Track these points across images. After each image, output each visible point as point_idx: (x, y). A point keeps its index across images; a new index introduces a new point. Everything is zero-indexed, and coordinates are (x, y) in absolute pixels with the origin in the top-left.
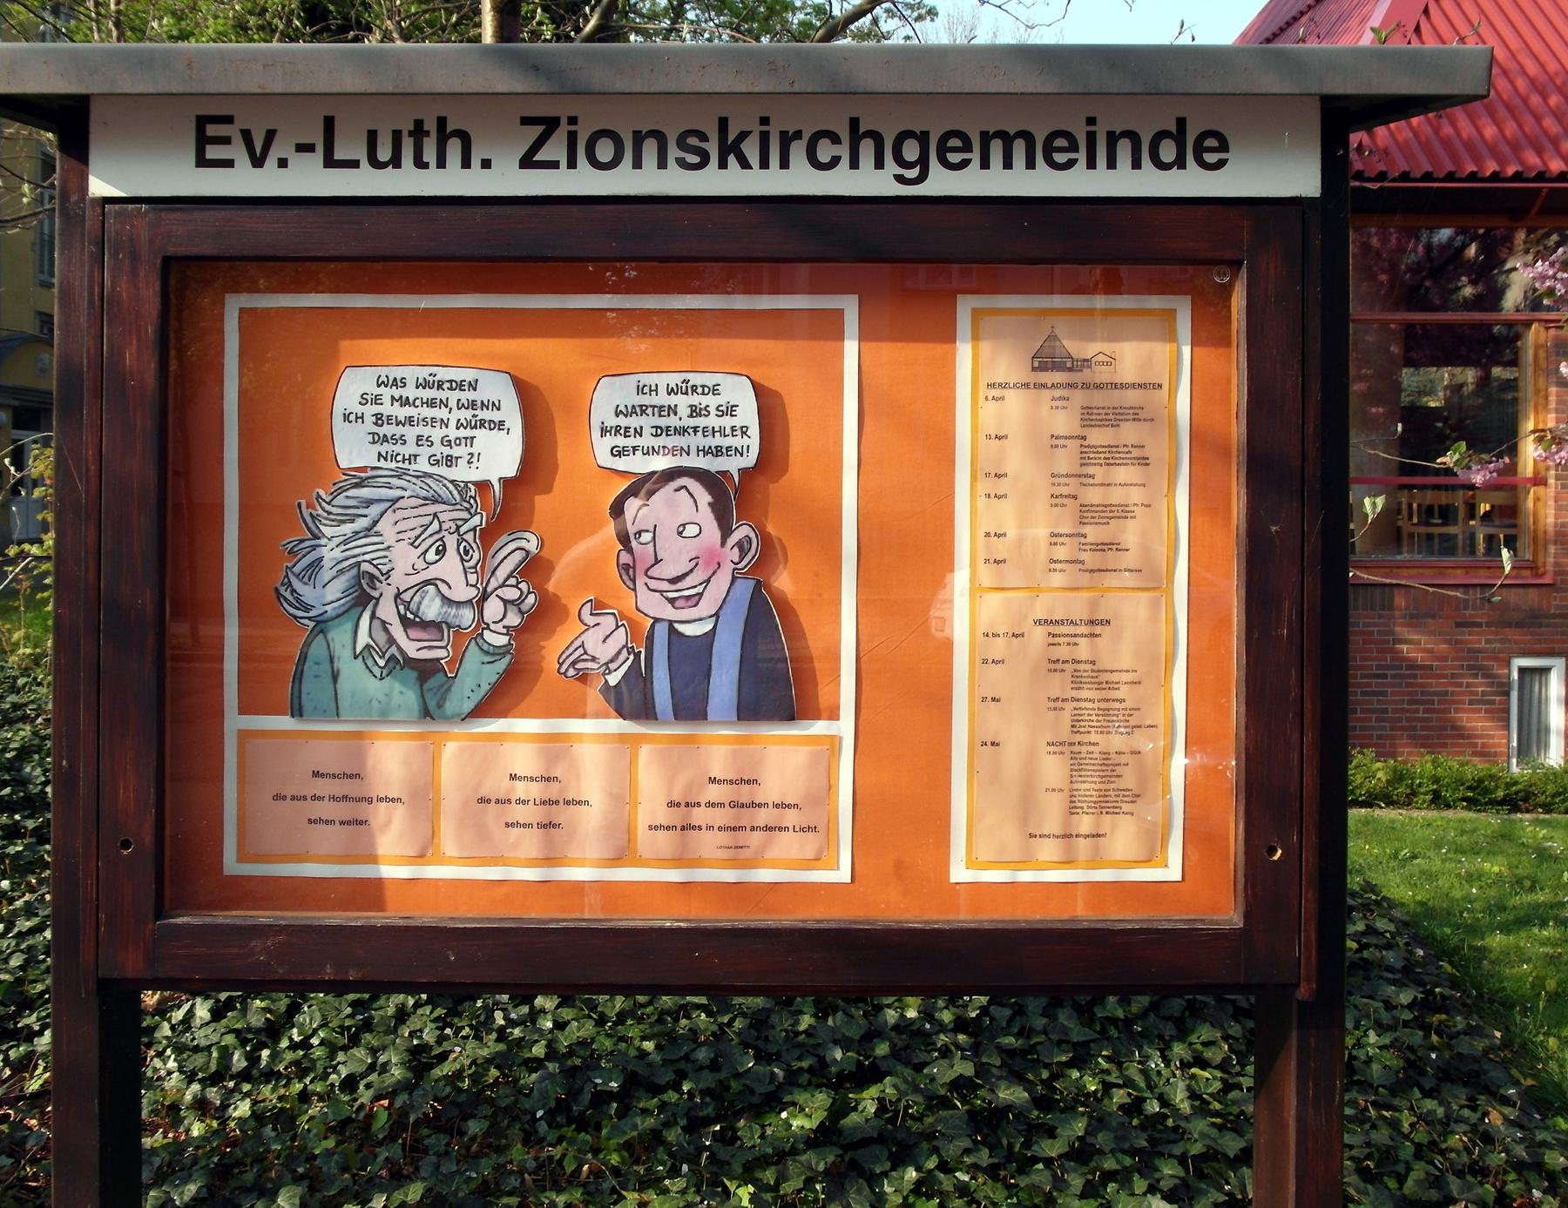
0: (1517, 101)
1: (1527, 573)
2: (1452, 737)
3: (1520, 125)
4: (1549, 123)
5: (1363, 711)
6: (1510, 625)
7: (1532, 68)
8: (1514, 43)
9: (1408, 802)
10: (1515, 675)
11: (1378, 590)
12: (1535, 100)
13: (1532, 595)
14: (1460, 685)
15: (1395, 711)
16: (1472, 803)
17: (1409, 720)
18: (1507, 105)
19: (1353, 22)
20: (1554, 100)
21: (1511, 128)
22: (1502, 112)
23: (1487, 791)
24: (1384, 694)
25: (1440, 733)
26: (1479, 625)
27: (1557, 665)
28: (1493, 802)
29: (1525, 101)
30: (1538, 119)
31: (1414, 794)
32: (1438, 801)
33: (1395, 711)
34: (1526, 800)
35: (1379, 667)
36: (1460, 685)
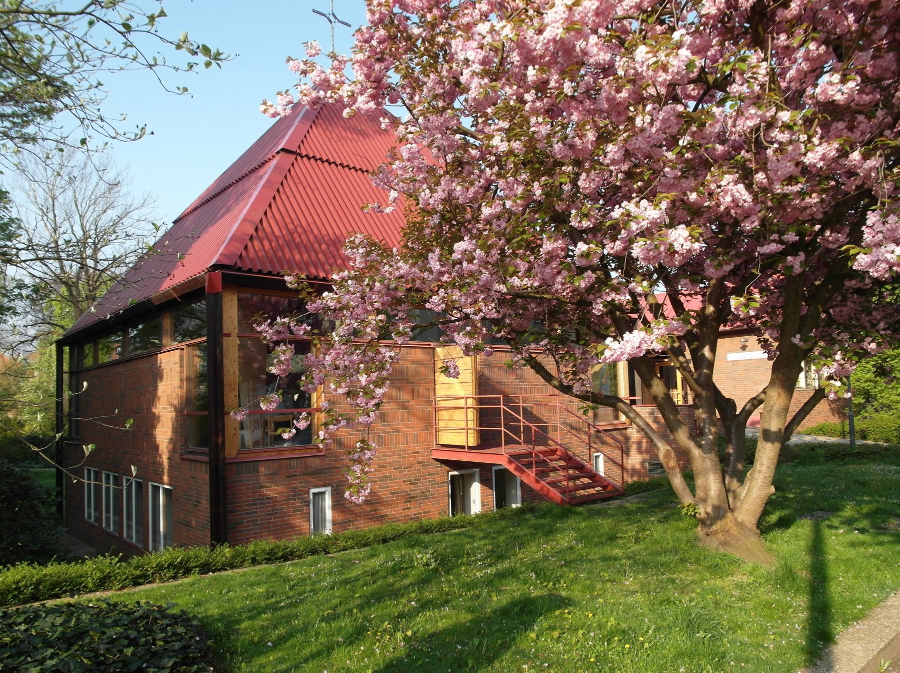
0: (309, 245)
1: (315, 451)
2: (287, 528)
3: (310, 256)
4: (321, 256)
5: (247, 522)
6: (308, 475)
7: (316, 232)
8: (339, 144)
9: (241, 565)
10: (311, 497)
11: (252, 464)
12: (316, 245)
13: (317, 460)
14: (289, 504)
15: (261, 520)
16: (269, 560)
17: (267, 523)
18: (305, 246)
19: (246, 196)
20: (324, 246)
21: (306, 257)
22: (303, 249)
23: (275, 554)
24: (256, 512)
25: (284, 529)
26: (296, 476)
27: (328, 490)
28: (278, 558)
29: (313, 247)
30: (317, 254)
31: (244, 561)
32: (254, 562)
33: (261, 520)
34: (291, 555)
35: (253, 500)
36: (289, 504)
